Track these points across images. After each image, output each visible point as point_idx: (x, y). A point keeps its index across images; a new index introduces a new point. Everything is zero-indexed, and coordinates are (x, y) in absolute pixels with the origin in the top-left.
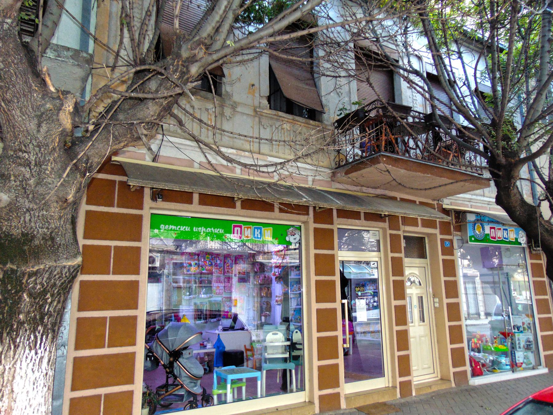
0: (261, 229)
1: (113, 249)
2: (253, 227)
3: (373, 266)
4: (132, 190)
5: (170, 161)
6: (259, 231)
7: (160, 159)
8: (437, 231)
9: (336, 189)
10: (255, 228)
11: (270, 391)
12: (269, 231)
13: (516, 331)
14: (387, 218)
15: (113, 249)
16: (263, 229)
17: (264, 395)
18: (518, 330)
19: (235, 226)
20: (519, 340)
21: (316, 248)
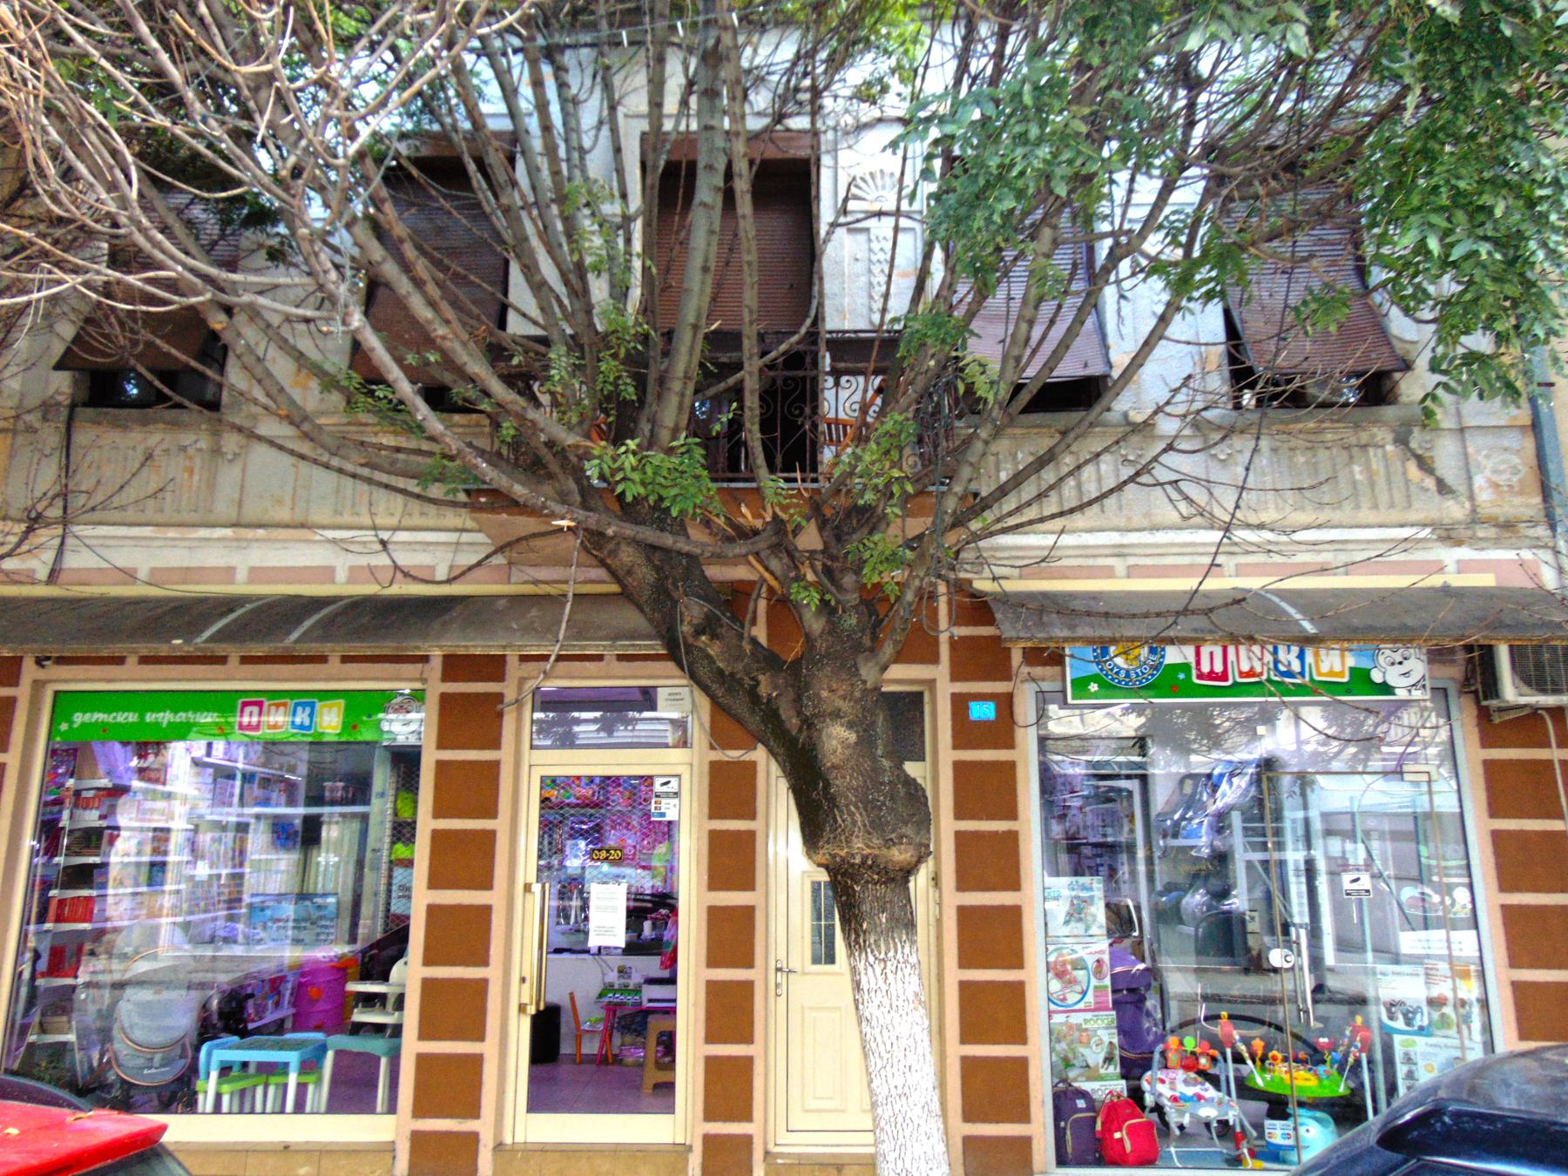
0: (312, 706)
1: (1557, 766)
2: (291, 703)
3: (665, 789)
4: (1497, 720)
5: (84, 577)
6: (308, 710)
7: (63, 577)
8: (940, 671)
9: (526, 582)
10: (297, 705)
11: (337, 1104)
12: (335, 710)
13: (1399, 1024)
14: (1484, 703)
15: (1557, 766)
16: (318, 705)
17: (323, 1107)
18: (1409, 1022)
19: (245, 704)
20: (1408, 1059)
21: (957, 745)
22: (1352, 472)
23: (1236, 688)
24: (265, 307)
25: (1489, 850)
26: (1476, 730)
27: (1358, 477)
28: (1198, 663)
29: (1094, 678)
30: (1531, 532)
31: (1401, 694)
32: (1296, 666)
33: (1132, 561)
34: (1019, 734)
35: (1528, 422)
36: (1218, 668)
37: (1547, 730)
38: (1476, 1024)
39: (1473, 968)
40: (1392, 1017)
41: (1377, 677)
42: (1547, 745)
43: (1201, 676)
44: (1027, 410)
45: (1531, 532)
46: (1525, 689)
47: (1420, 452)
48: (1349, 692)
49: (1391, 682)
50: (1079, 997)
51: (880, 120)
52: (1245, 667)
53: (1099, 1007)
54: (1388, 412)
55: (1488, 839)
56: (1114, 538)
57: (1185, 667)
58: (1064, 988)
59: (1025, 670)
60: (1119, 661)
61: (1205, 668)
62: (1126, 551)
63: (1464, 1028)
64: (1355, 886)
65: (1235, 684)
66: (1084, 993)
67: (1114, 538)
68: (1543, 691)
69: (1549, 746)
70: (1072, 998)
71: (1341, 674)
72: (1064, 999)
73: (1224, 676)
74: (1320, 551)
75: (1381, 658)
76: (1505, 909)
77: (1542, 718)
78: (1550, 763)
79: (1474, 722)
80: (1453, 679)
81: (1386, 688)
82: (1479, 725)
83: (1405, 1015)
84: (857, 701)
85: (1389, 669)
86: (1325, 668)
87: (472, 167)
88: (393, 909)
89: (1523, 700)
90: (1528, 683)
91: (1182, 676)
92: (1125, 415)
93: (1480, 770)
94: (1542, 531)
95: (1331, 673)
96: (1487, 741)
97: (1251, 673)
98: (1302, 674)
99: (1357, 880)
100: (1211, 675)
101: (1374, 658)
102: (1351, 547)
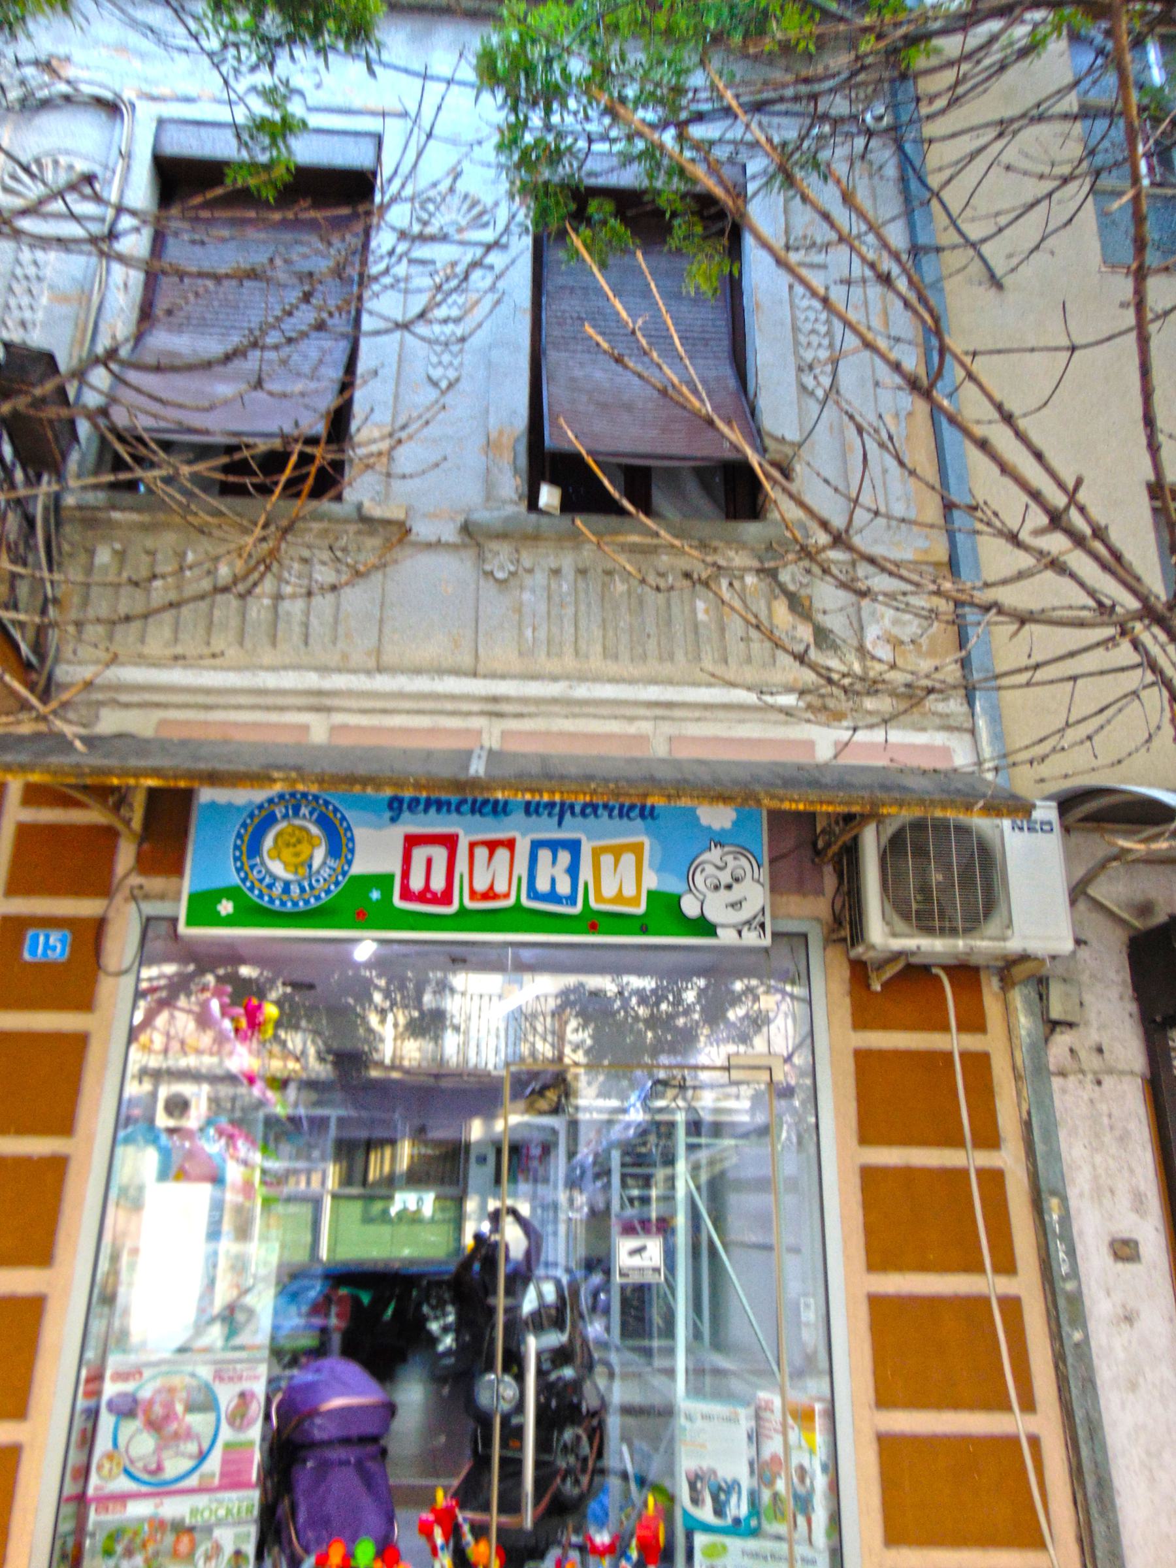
13: (706, 1513)
18: (719, 1511)
22: (694, 611)
23: (464, 919)
24: (911, 936)
25: (855, 1198)
26: (847, 1001)
27: (701, 616)
28: (406, 874)
29: (230, 893)
30: (941, 707)
31: (726, 937)
32: (564, 888)
33: (339, 718)
34: (106, 986)
35: (945, 558)
36: (438, 884)
37: (945, 999)
38: (820, 1516)
39: (818, 1407)
40: (696, 1501)
41: (690, 907)
42: (945, 1028)
43: (406, 894)
44: (103, 441)
45: (941, 707)
46: (900, 925)
47: (792, 587)
48: (644, 930)
49: (711, 916)
50: (188, 1464)
51: (67, 98)
52: (481, 886)
53: (231, 1480)
54: (751, 530)
55: (856, 1180)
56: (312, 680)
57: (383, 881)
58: (159, 1449)
59: (136, 880)
60: (277, 868)
61: (416, 884)
62: (328, 702)
63: (801, 1520)
64: (636, 1261)
65: (463, 912)
66: (202, 1456)
67: (312, 680)
68: (928, 931)
69: (946, 1028)
70: (174, 1466)
71: (635, 901)
72: (159, 1469)
73: (446, 897)
74: (632, 719)
75: (699, 879)
76: (876, 1302)
77: (937, 978)
78: (948, 1056)
79: (846, 987)
80: (818, 919)
81: (704, 927)
82: (851, 993)
83: (715, 1499)
84: (393, 1004)
85: (710, 896)
86: (609, 890)
87: (197, 491)
88: (772, 1197)
89: (897, 944)
90: (906, 916)
91: (375, 895)
92: (359, 507)
93: (849, 1065)
94: (955, 706)
95: (619, 898)
96: (861, 1021)
97: (489, 895)
98: (572, 899)
99: (639, 1251)
100: (426, 896)
101: (688, 878)
102: (677, 713)
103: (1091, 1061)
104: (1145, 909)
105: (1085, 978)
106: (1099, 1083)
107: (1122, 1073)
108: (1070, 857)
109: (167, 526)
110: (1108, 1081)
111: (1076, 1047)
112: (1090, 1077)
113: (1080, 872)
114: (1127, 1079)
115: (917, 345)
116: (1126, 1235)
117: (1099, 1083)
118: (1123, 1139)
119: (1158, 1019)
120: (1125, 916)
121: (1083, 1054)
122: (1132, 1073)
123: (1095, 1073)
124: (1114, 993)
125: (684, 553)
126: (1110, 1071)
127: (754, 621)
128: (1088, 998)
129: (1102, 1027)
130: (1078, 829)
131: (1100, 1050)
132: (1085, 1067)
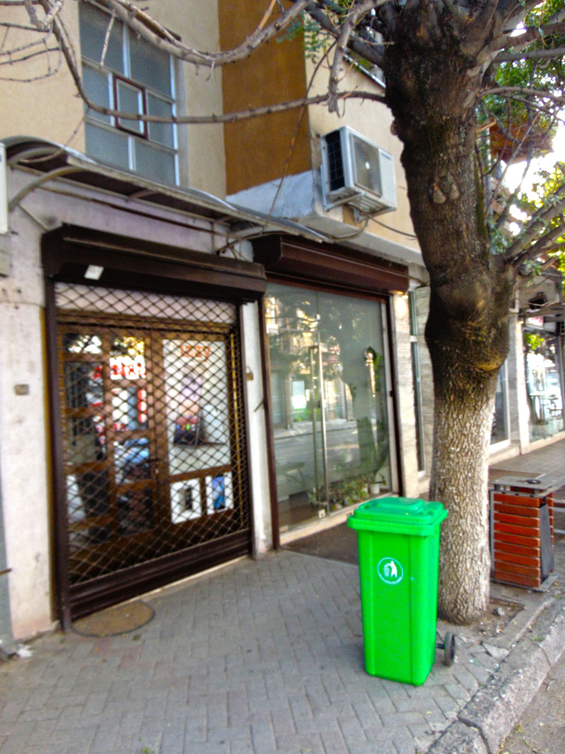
103: (15, 297)
104: (51, 221)
105: (15, 252)
106: (17, 308)
107: (30, 304)
108: (9, 183)
109: (68, 404)
110: (22, 307)
111: (7, 289)
112: (12, 305)
113: (15, 193)
114: (32, 307)
115: (272, 209)
116: (23, 382)
117: (17, 308)
118: (27, 336)
119: (51, 276)
120: (40, 221)
121: (10, 293)
122: (35, 304)
123: (15, 302)
124: (30, 262)
125: (29, 159)
126: (24, 302)
127: (506, 603)
128: (15, 263)
129: (22, 279)
130: (18, 169)
131: (19, 291)
132: (11, 299)
